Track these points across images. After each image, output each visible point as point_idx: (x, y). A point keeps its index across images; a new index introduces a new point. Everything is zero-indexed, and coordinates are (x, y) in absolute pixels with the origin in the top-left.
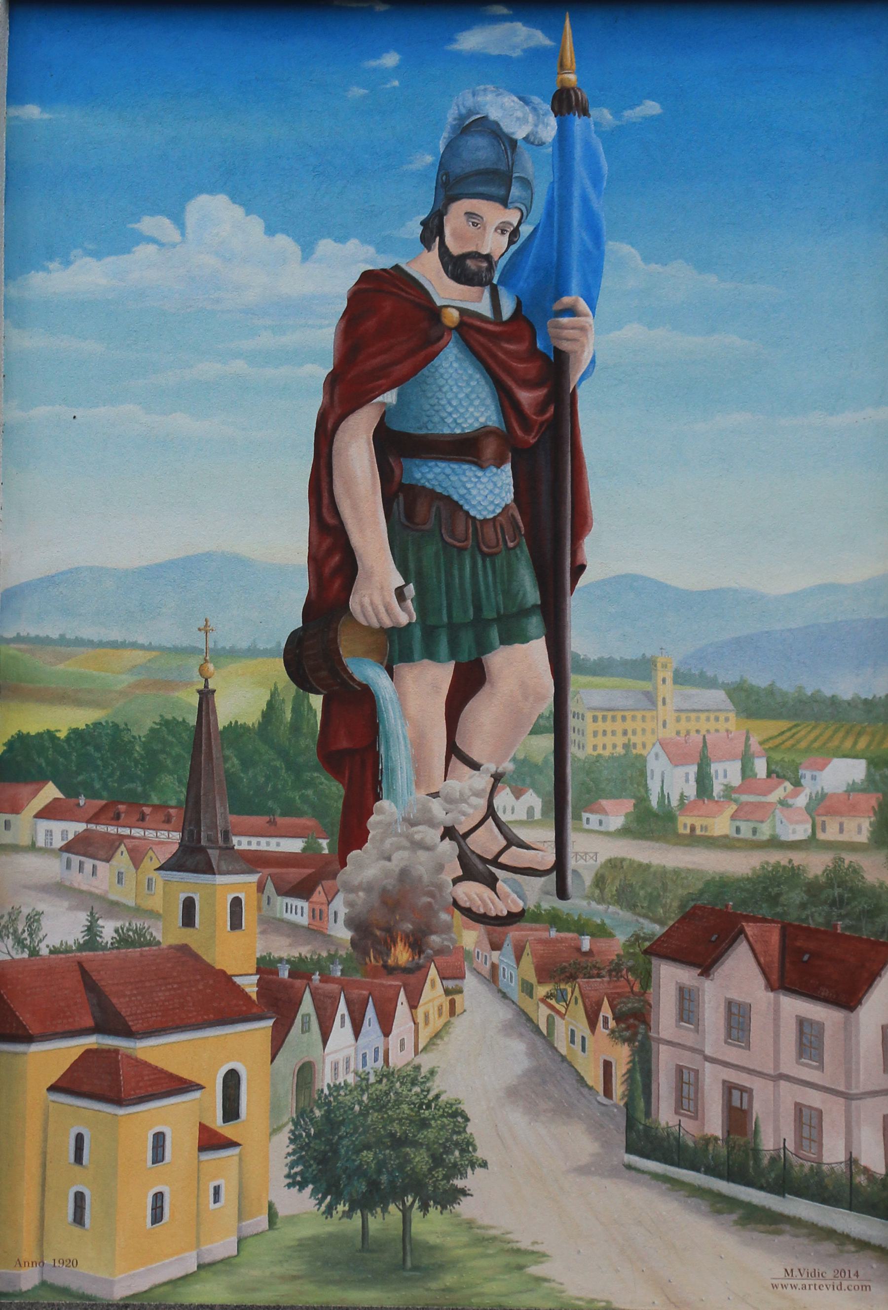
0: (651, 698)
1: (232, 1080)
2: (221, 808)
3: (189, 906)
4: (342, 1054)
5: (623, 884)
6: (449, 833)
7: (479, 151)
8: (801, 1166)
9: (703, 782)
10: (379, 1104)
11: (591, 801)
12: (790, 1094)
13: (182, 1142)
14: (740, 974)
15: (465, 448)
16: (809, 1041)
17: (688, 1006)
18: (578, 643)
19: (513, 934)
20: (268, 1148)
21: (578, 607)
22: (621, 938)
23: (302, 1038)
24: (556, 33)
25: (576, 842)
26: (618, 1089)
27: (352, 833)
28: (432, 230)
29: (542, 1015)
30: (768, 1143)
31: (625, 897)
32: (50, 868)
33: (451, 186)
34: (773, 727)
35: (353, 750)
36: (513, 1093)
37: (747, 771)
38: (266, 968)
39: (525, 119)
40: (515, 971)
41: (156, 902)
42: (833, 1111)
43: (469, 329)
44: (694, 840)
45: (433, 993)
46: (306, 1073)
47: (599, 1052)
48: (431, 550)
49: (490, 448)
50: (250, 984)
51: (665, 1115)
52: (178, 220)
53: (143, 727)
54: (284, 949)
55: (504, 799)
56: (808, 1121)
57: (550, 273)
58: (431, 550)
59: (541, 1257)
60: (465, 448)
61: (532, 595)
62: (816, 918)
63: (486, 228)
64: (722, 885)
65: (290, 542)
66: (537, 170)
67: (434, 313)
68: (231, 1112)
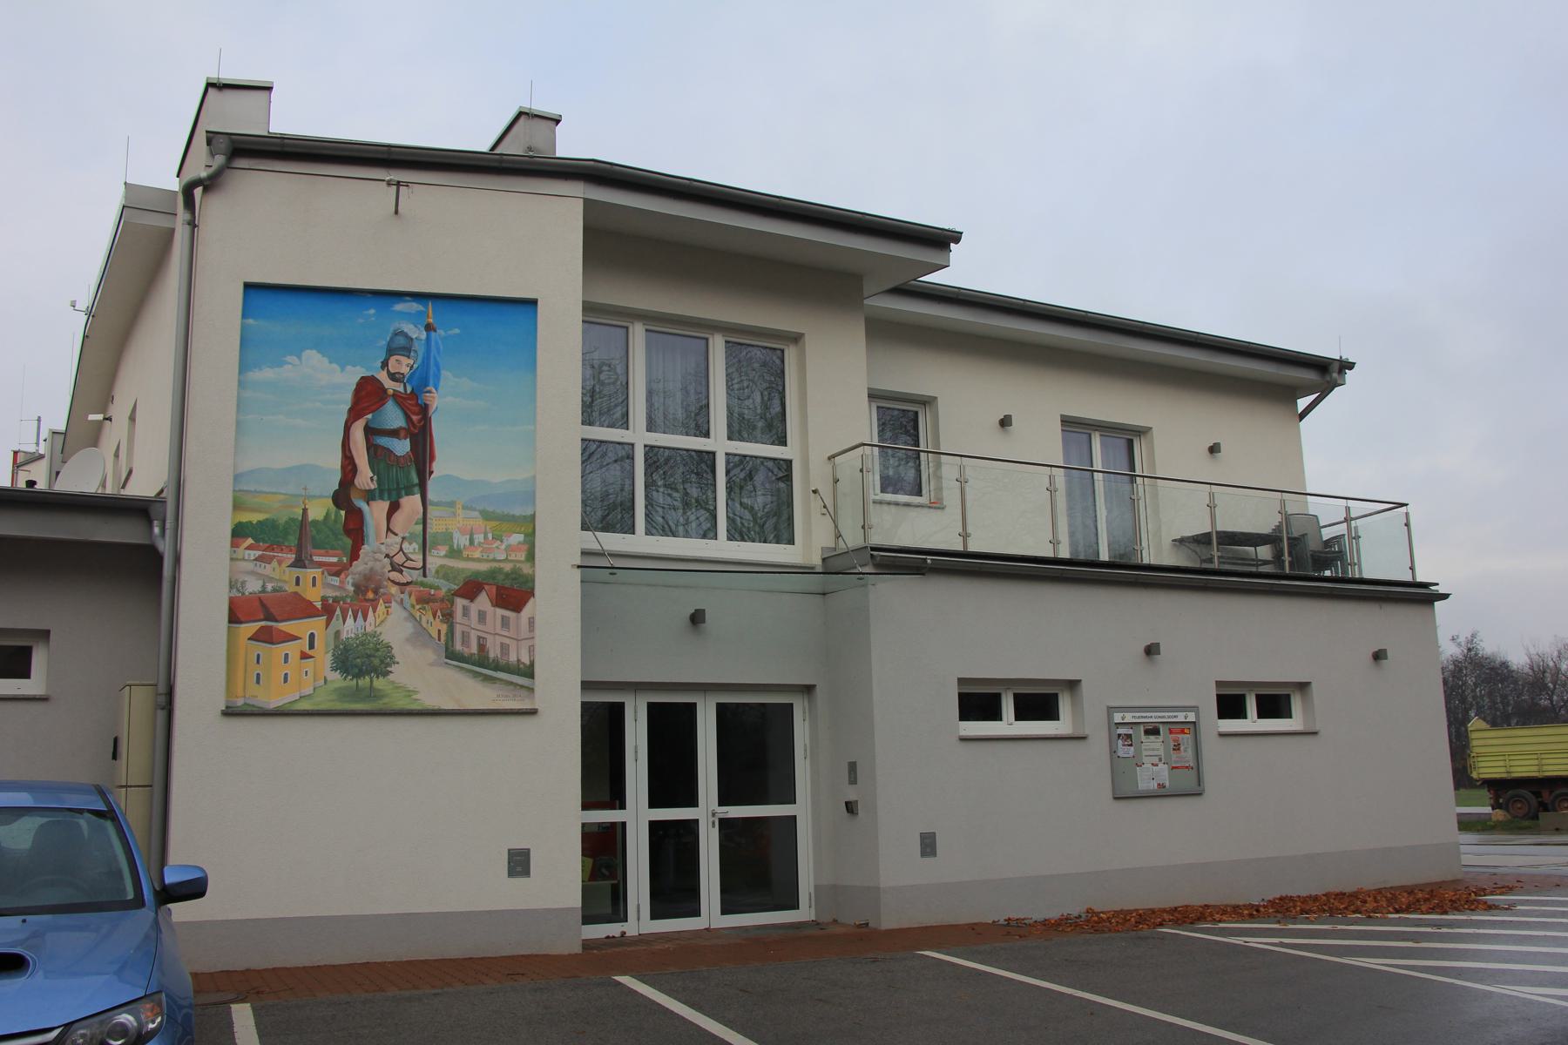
0: (454, 514)
1: (312, 636)
2: (309, 547)
3: (298, 579)
4: (350, 628)
5: (444, 572)
6: (387, 556)
7: (401, 341)
8: (502, 662)
9: (471, 541)
10: (362, 644)
11: (435, 545)
12: (499, 640)
13: (294, 656)
14: (483, 601)
15: (394, 433)
16: (505, 622)
17: (466, 611)
18: (431, 496)
19: (408, 589)
20: (324, 658)
21: (430, 484)
22: (444, 590)
23: (336, 622)
24: (426, 306)
25: (429, 559)
26: (443, 638)
27: (354, 556)
28: (385, 364)
29: (418, 615)
30: (492, 655)
31: (446, 577)
32: (250, 566)
33: (391, 351)
34: (494, 523)
35: (355, 529)
36: (407, 640)
37: (486, 538)
38: (324, 600)
39: (416, 332)
40: (409, 601)
41: (286, 578)
42: (513, 645)
43: (396, 396)
44: (468, 559)
45: (381, 607)
46: (337, 634)
47: (436, 626)
48: (382, 465)
49: (402, 434)
50: (319, 605)
51: (458, 647)
52: (299, 357)
53: (282, 521)
54: (331, 593)
55: (405, 546)
56: (505, 648)
57: (423, 380)
58: (382, 465)
59: (416, 692)
60: (394, 433)
61: (416, 480)
62: (508, 584)
63: (402, 365)
64: (478, 573)
65: (335, 462)
66: (419, 348)
67: (385, 391)
68: (312, 646)
